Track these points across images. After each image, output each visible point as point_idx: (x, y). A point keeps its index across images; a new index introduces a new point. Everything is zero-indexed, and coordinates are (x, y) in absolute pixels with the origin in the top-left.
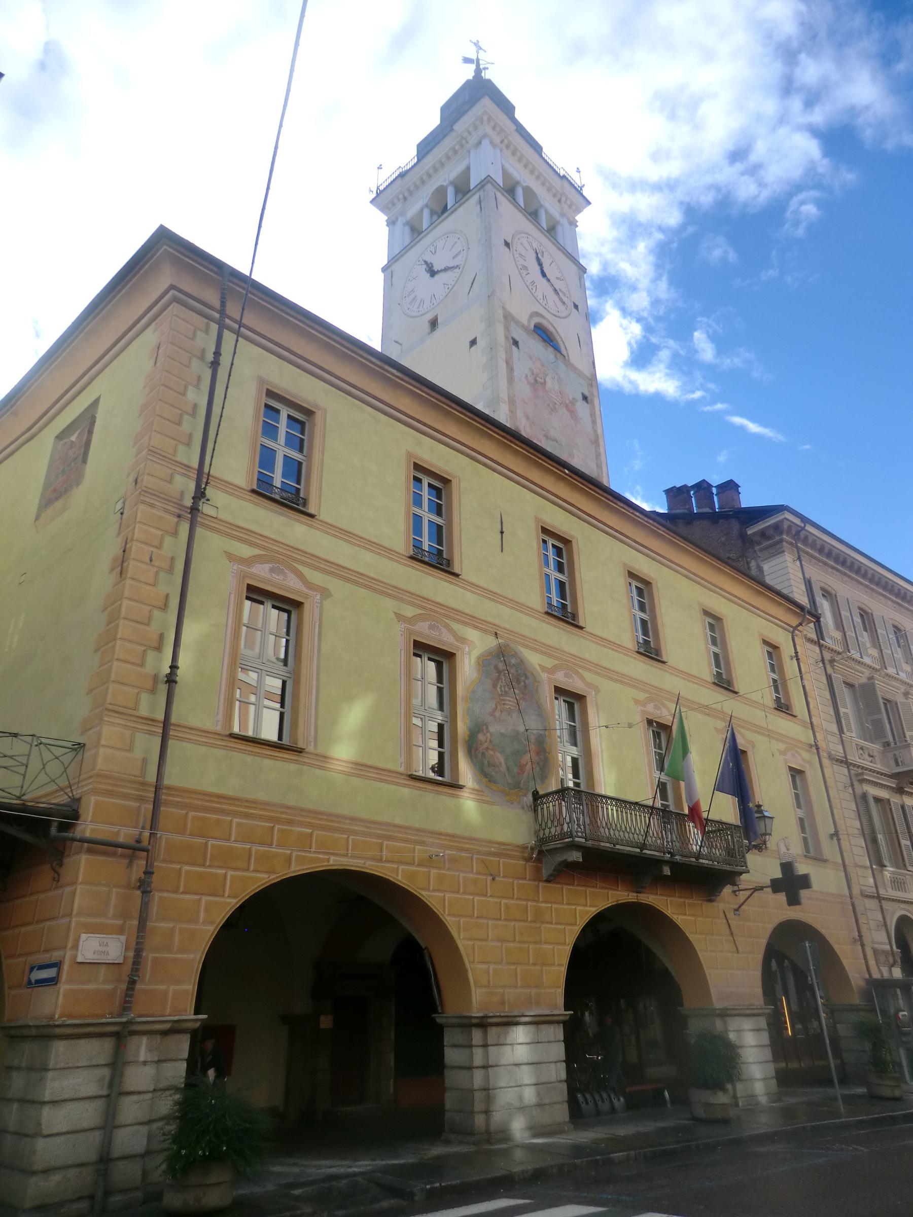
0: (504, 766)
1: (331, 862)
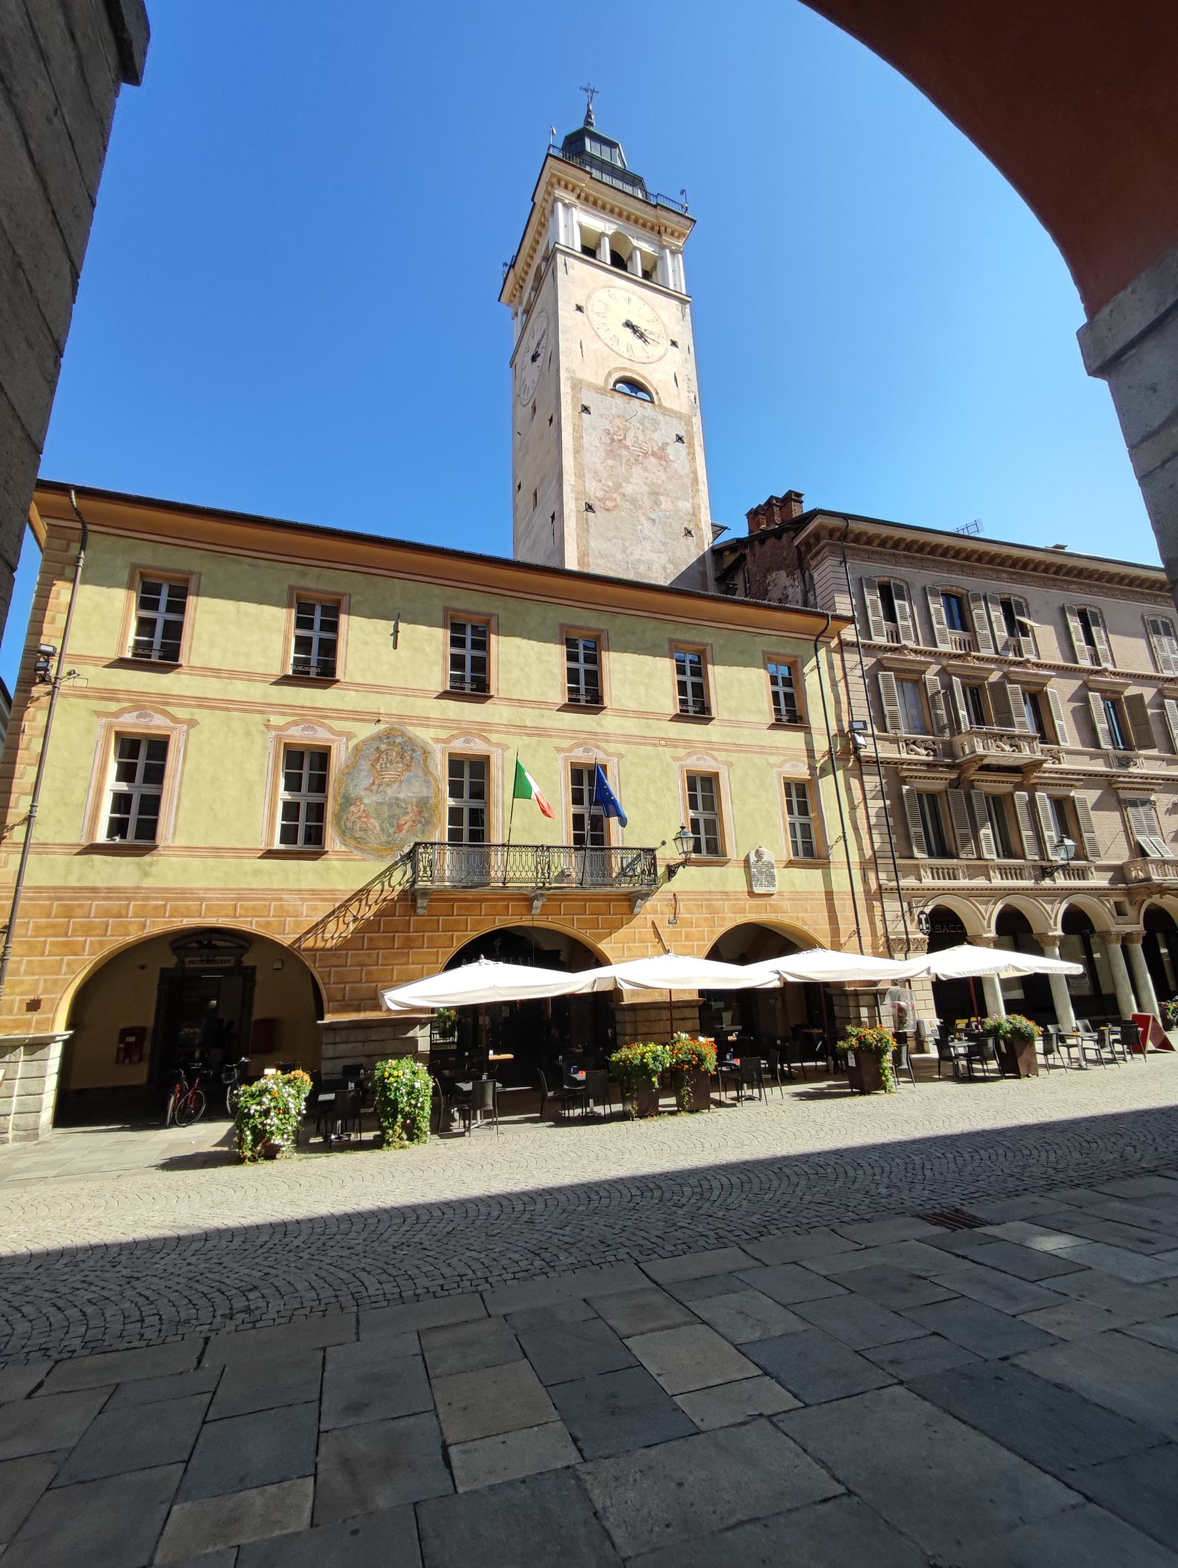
0: (378, 828)
1: (184, 923)
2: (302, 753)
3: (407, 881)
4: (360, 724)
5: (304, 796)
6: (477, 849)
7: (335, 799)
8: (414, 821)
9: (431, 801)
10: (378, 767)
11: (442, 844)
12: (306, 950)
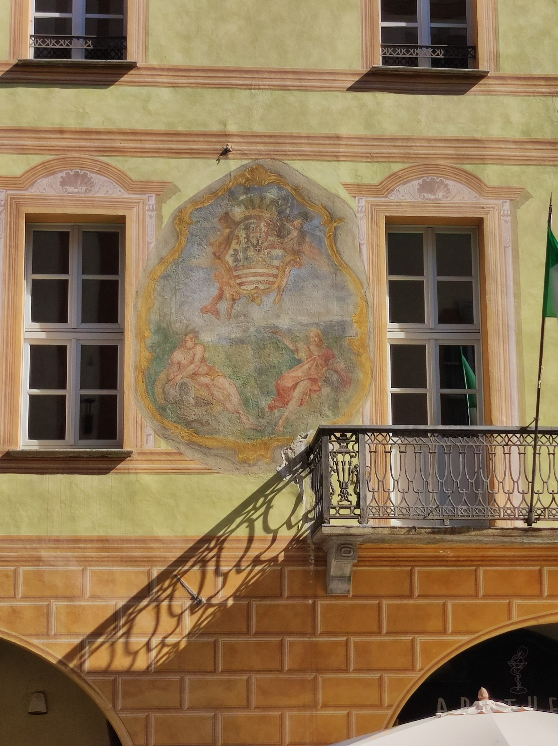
0: (235, 398)
2: (64, 237)
3: (305, 518)
4: (183, 163)
5: (432, 331)
6: (460, 442)
7: (140, 336)
8: (314, 381)
9: (351, 332)
10: (229, 259)
11: (380, 431)
12: (91, 673)
